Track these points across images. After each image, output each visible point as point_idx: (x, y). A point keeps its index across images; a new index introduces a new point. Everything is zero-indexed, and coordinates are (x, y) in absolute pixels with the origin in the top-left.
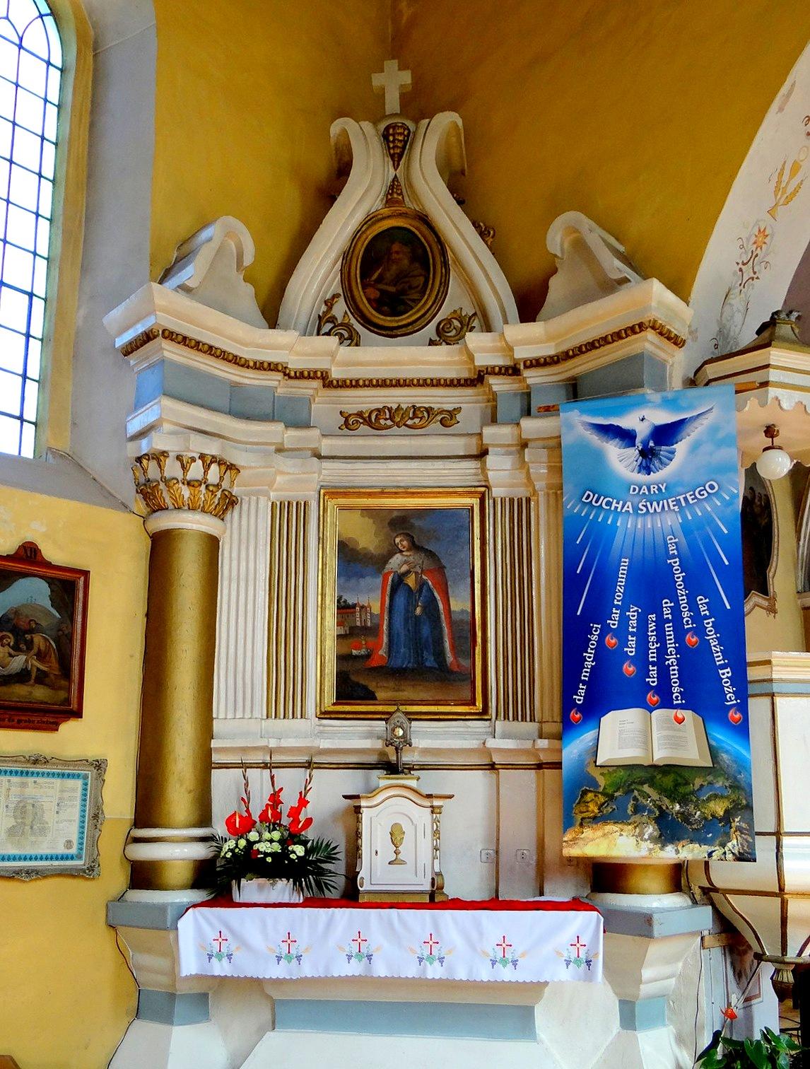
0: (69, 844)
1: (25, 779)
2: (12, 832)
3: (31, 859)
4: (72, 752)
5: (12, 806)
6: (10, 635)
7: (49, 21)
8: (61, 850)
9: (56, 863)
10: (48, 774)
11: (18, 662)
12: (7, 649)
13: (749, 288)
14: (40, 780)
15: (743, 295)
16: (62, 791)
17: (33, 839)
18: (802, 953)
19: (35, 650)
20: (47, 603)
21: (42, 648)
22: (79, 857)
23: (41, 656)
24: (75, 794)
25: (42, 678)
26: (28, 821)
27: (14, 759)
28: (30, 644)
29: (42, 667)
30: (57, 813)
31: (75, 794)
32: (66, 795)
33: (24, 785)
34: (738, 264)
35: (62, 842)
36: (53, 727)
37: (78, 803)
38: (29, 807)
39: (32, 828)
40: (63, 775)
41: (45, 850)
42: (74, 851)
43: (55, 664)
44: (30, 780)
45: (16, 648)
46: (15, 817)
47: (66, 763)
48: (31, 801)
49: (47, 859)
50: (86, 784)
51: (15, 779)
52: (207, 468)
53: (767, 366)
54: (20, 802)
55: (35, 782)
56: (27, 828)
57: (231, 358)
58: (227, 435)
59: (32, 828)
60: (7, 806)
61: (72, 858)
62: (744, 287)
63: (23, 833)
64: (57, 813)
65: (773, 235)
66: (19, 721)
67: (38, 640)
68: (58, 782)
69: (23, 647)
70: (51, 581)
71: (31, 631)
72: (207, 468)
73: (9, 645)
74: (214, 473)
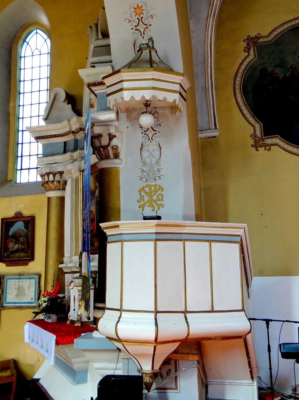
0: (32, 299)
1: (19, 280)
2: (17, 295)
3: (22, 303)
4: (32, 271)
5: (16, 288)
6: (14, 239)
7: (27, 40)
8: (30, 301)
9: (28, 304)
10: (25, 278)
11: (16, 246)
12: (13, 244)
13: (147, 33)
14: (23, 280)
15: (145, 38)
16: (29, 283)
17: (22, 297)
18: (175, 362)
19: (20, 243)
20: (23, 228)
21: (22, 241)
22: (35, 303)
23: (22, 244)
24: (33, 284)
25: (23, 250)
26: (21, 292)
27: (15, 274)
28: (19, 241)
29: (22, 247)
30: (28, 289)
31: (33, 284)
32: (30, 284)
33: (19, 282)
34: (133, 29)
35: (30, 298)
36: (27, 264)
37: (34, 286)
38: (21, 288)
39: (21, 294)
40: (30, 278)
41: (25, 301)
42: (33, 301)
43: (26, 245)
44: (21, 280)
45: (16, 243)
46: (17, 291)
47: (30, 274)
48: (21, 286)
49: (26, 303)
50: (36, 281)
51: (17, 280)
52: (48, 177)
53: (122, 81)
54: (18, 287)
55: (22, 281)
56: (20, 294)
57: (49, 136)
58: (58, 162)
59: (21, 294)
60: (15, 288)
61: (33, 303)
62: (144, 34)
63: (19, 296)
64: (28, 289)
65: (145, 5)
66: (16, 264)
67: (21, 239)
68: (28, 280)
69: (18, 242)
70: (24, 221)
71: (20, 237)
72: (54, 176)
73: (14, 242)
74: (58, 177)
